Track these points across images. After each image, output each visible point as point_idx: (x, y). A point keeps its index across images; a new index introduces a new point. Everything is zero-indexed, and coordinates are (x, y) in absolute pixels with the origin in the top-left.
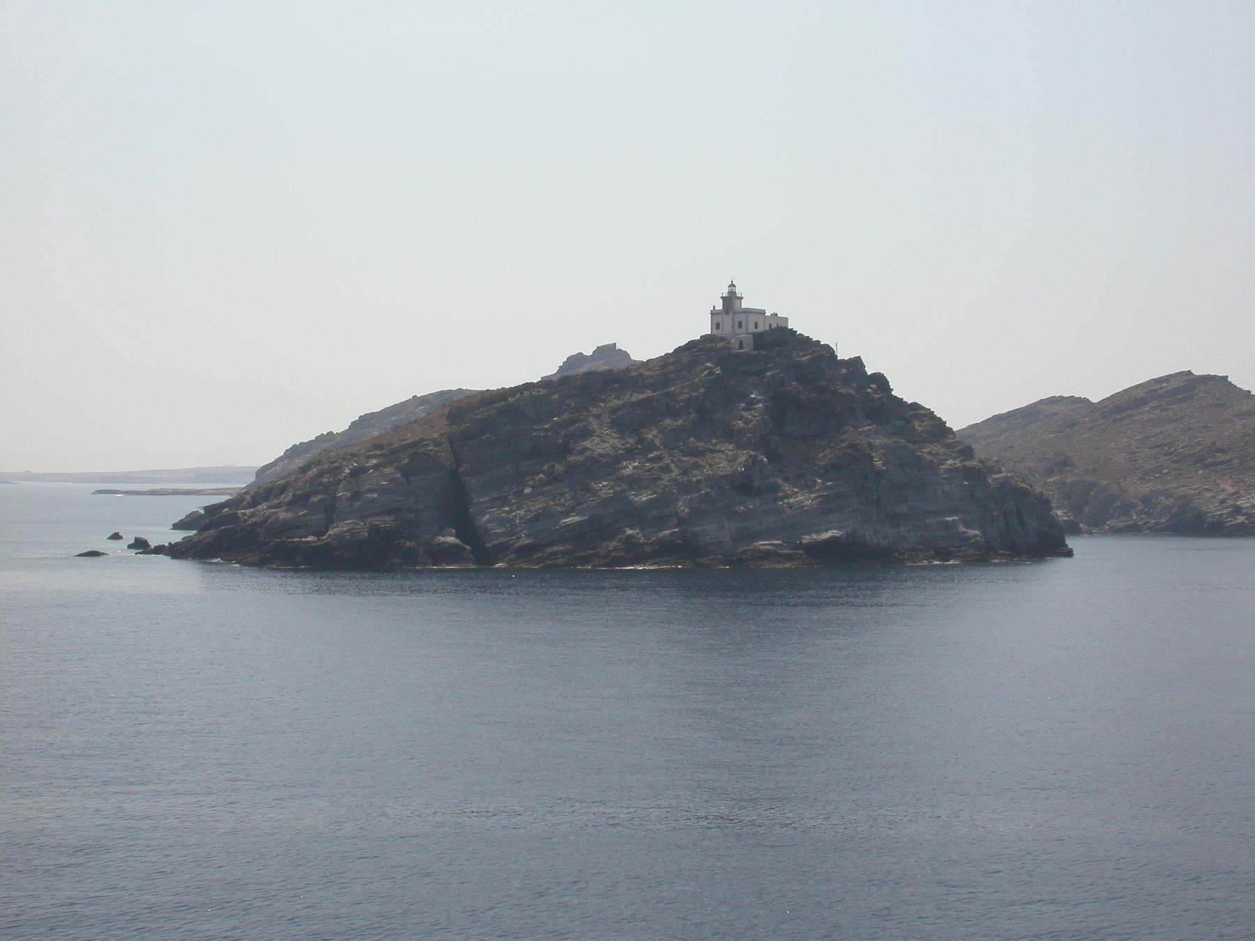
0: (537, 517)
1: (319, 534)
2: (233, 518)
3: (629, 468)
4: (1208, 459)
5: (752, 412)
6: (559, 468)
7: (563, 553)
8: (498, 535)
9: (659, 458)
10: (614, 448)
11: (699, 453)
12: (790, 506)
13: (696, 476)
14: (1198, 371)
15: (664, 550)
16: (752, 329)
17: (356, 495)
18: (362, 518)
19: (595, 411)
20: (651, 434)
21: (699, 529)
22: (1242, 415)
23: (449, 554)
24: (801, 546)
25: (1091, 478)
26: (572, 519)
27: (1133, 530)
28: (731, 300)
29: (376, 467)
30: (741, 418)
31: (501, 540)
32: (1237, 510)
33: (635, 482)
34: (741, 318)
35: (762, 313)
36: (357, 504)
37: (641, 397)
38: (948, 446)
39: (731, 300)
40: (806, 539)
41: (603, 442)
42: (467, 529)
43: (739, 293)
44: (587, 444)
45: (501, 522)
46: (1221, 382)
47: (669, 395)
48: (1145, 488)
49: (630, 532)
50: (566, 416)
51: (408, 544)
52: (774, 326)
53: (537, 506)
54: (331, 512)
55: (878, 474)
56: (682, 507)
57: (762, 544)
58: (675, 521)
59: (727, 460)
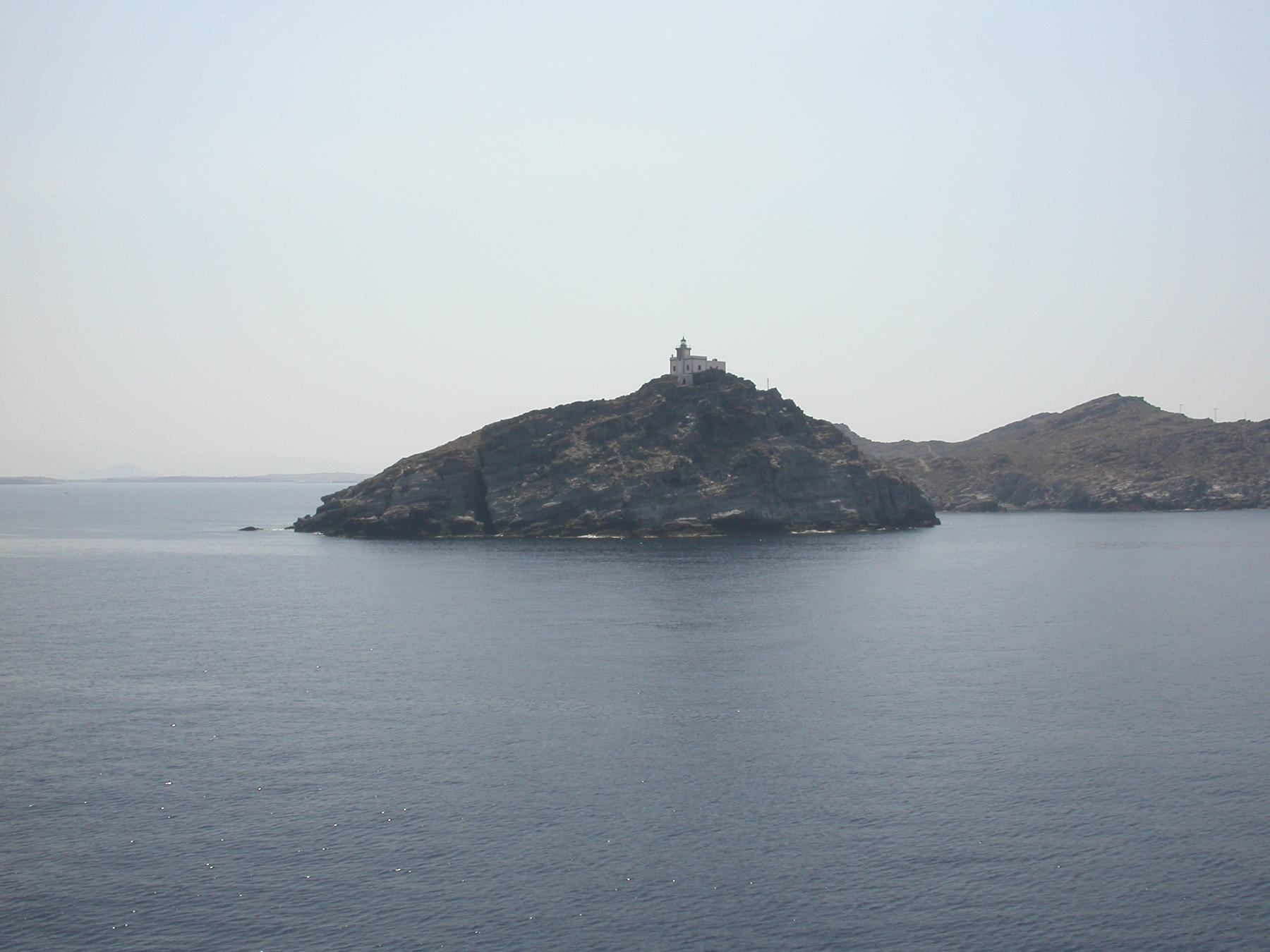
0: (527, 503)
1: (379, 515)
2: (337, 504)
3: (594, 468)
4: (1104, 458)
5: (685, 430)
6: (547, 468)
7: (541, 527)
8: (501, 515)
9: (616, 461)
10: (586, 454)
11: (645, 457)
12: (705, 493)
13: (639, 473)
14: (1123, 395)
15: (610, 525)
16: (696, 370)
17: (405, 489)
18: (408, 504)
19: (577, 429)
20: (613, 445)
21: (636, 510)
22: (1148, 425)
23: (466, 528)
24: (710, 521)
25: (1020, 472)
26: (552, 503)
27: (1044, 508)
28: (683, 350)
29: (421, 469)
30: (677, 432)
31: (504, 518)
32: (1113, 493)
33: (595, 478)
34: (688, 363)
35: (705, 359)
36: (406, 495)
37: (607, 418)
38: (840, 450)
39: (683, 350)
40: (714, 516)
41: (579, 450)
42: (483, 513)
43: (688, 345)
44: (567, 452)
45: (504, 506)
46: (1137, 404)
47: (629, 418)
48: (1056, 478)
49: (588, 512)
50: (556, 433)
51: (434, 521)
52: (703, 369)
53: (527, 495)
54: (388, 500)
55: (775, 471)
56: (627, 496)
57: (681, 520)
58: (621, 504)
59: (664, 460)
